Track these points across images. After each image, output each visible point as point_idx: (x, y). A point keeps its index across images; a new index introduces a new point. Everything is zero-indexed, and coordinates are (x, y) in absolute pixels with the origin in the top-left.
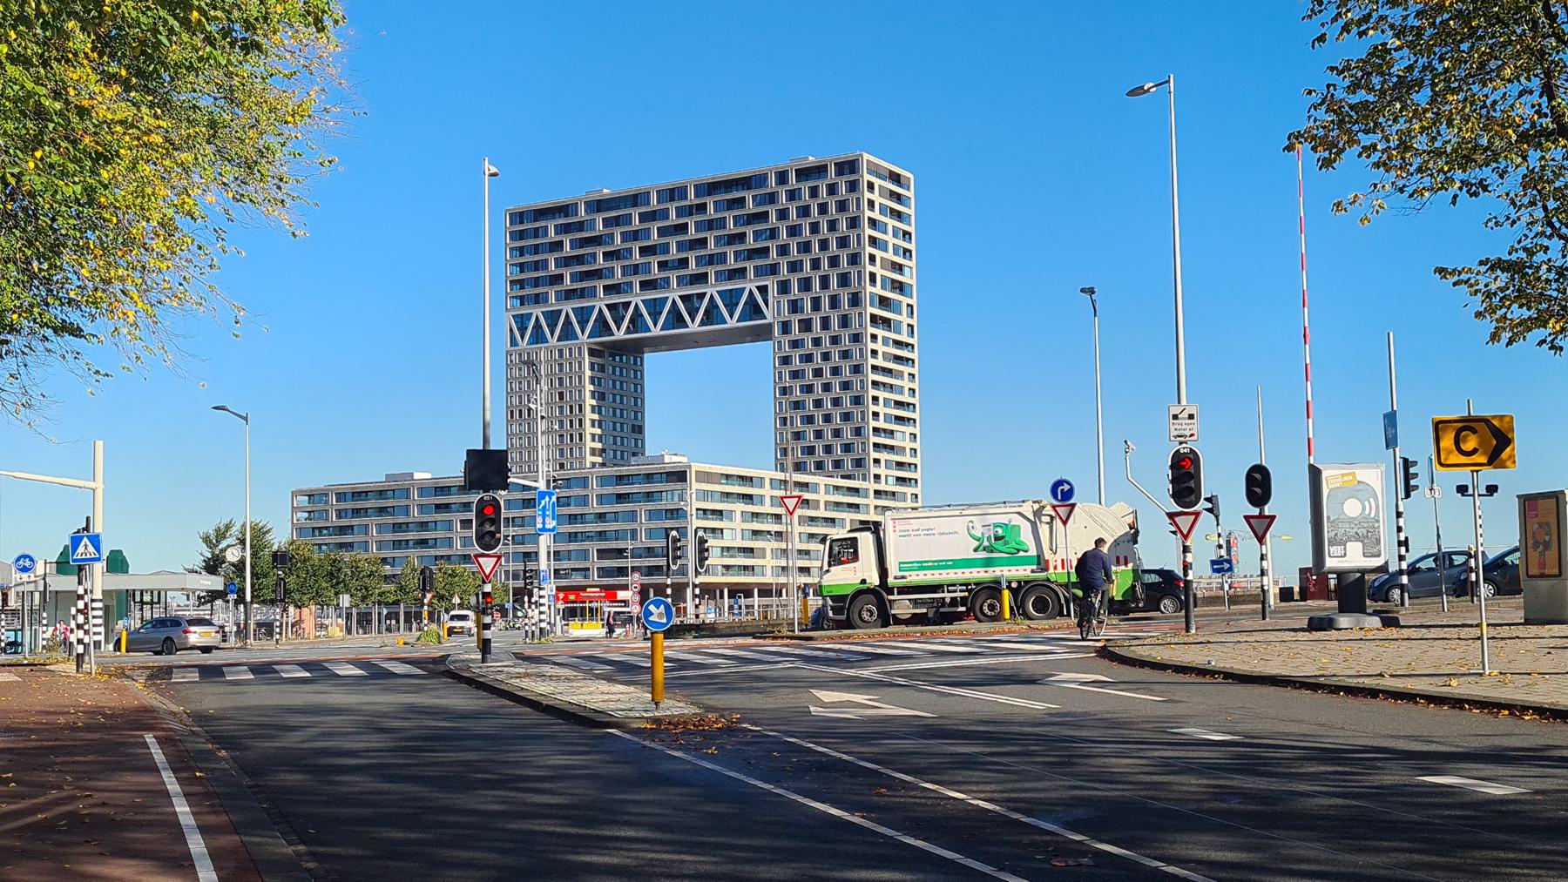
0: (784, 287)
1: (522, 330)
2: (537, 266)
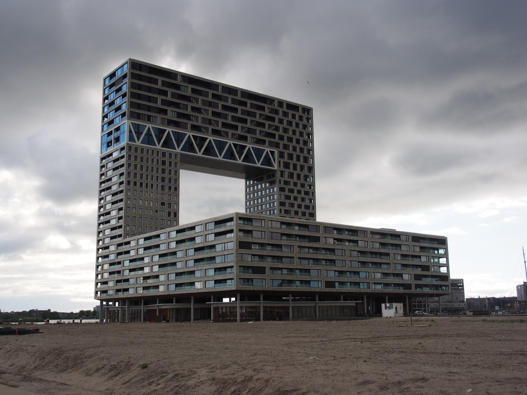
0: (281, 155)
1: (139, 134)
2: (149, 99)
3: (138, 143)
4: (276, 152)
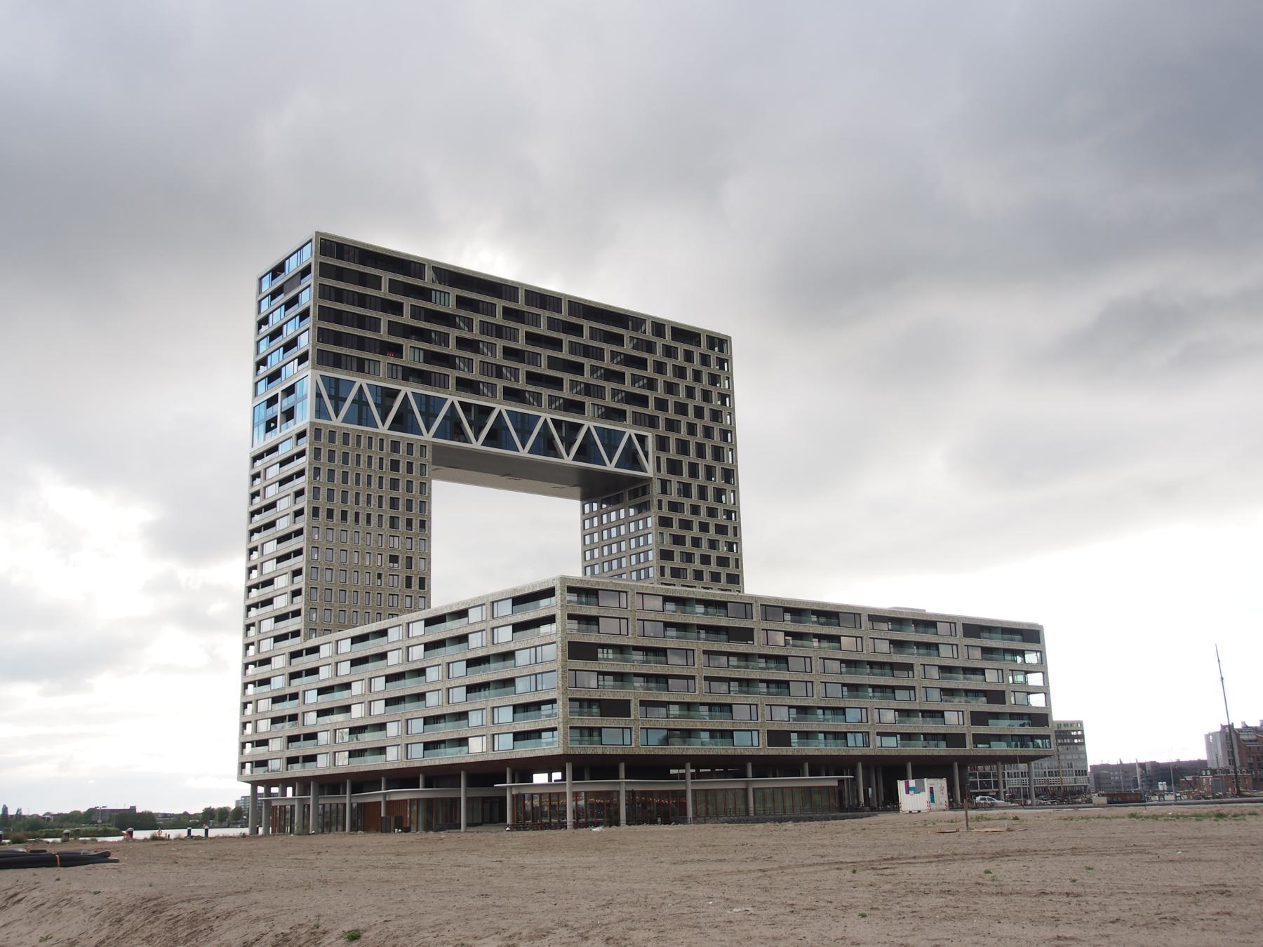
0: (662, 444)
1: (338, 401)
2: (361, 322)
3: (336, 422)
4: (650, 436)
